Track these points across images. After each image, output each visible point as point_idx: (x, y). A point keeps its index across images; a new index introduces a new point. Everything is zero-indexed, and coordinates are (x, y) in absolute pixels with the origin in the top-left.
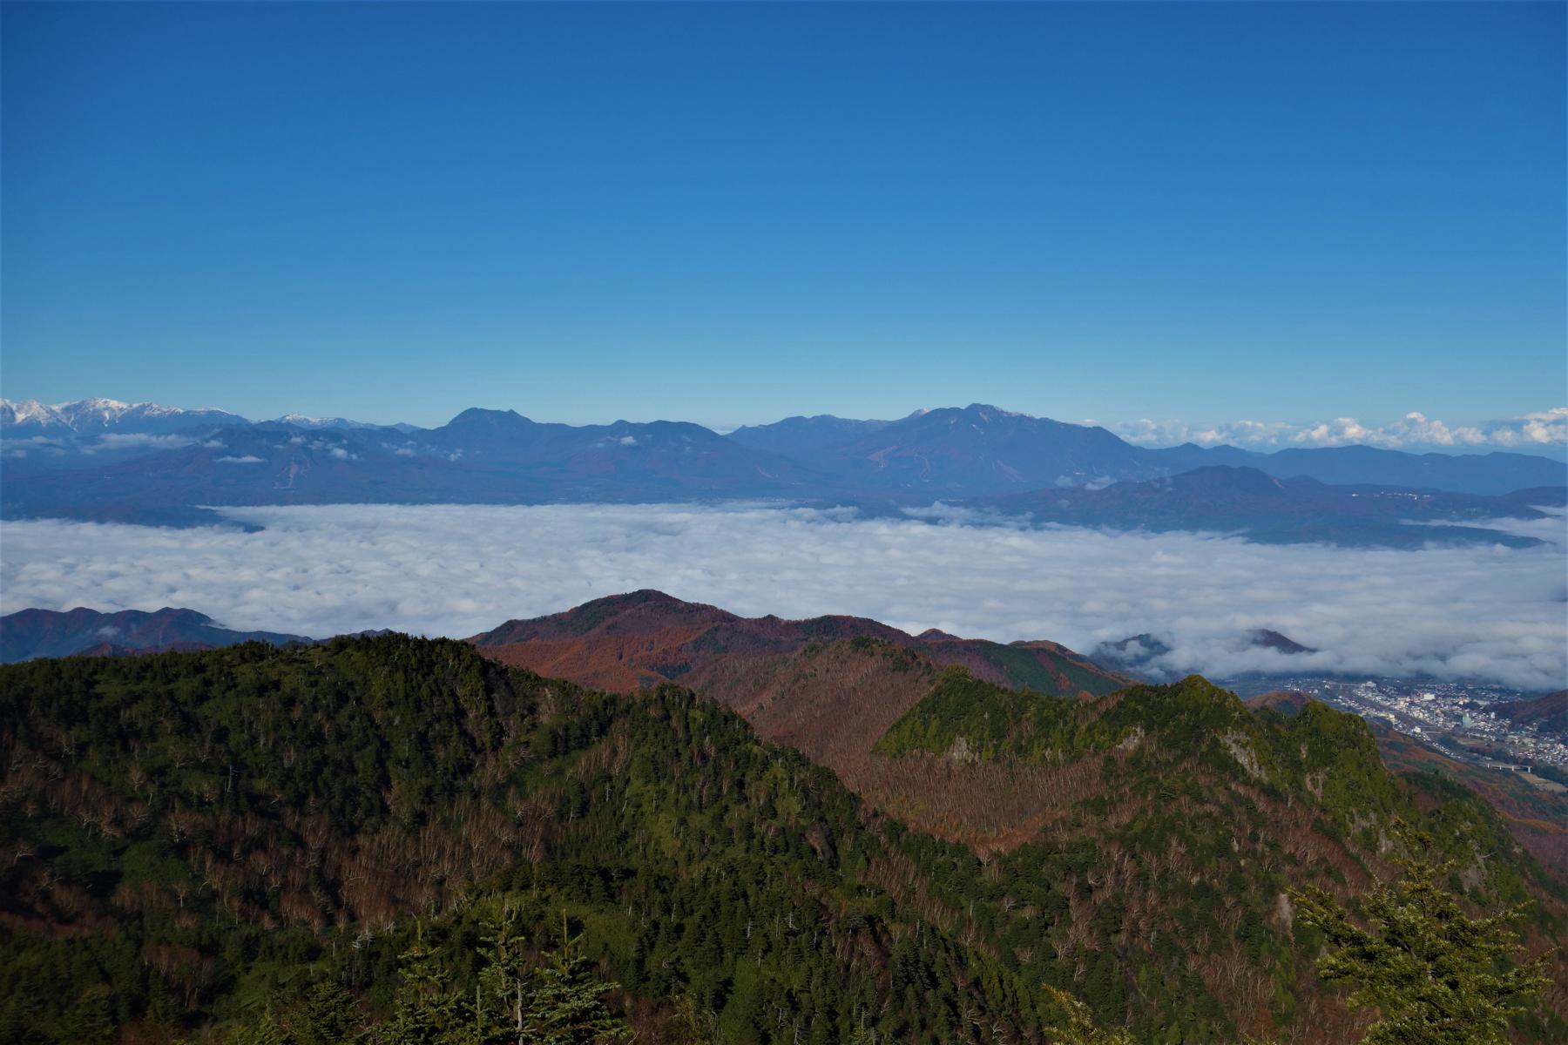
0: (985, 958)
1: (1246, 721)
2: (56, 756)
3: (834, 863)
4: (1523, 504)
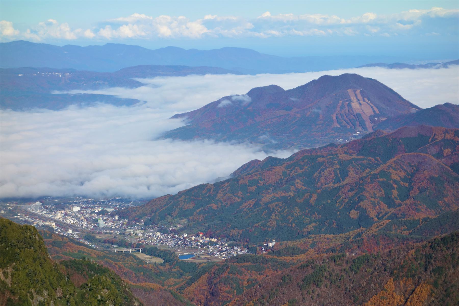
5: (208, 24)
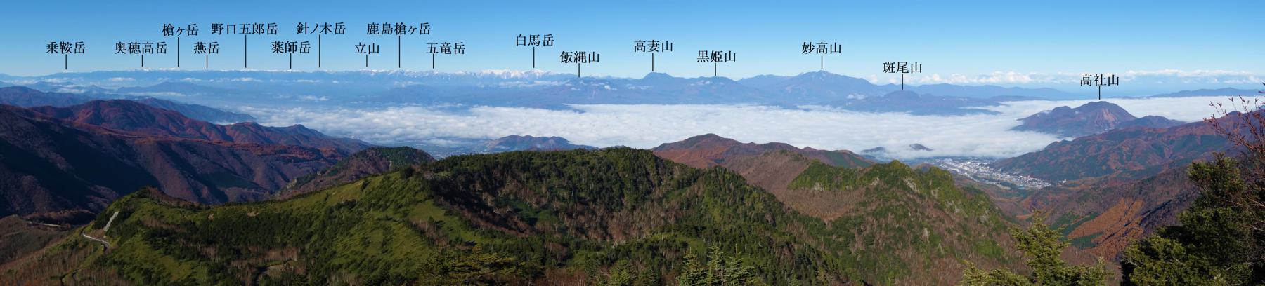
0: (827, 254)
1: (912, 174)
2: (520, 181)
3: (774, 225)
4: (995, 101)
5: (1031, 76)
